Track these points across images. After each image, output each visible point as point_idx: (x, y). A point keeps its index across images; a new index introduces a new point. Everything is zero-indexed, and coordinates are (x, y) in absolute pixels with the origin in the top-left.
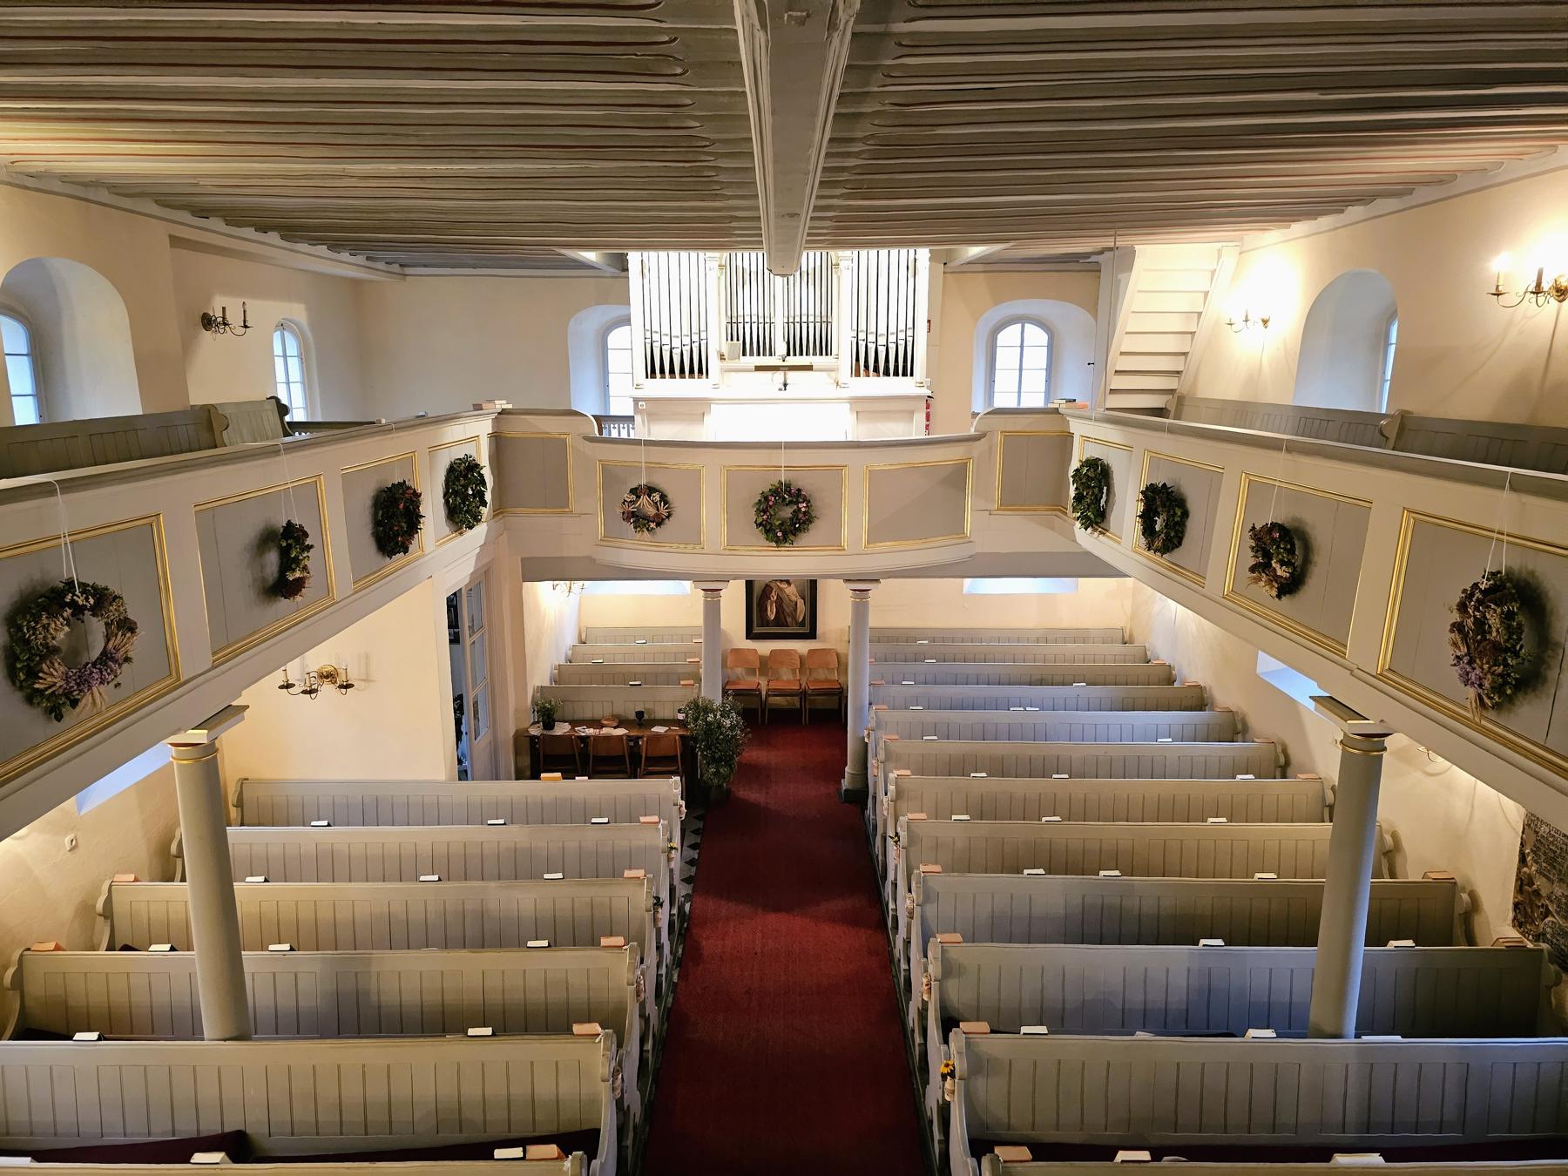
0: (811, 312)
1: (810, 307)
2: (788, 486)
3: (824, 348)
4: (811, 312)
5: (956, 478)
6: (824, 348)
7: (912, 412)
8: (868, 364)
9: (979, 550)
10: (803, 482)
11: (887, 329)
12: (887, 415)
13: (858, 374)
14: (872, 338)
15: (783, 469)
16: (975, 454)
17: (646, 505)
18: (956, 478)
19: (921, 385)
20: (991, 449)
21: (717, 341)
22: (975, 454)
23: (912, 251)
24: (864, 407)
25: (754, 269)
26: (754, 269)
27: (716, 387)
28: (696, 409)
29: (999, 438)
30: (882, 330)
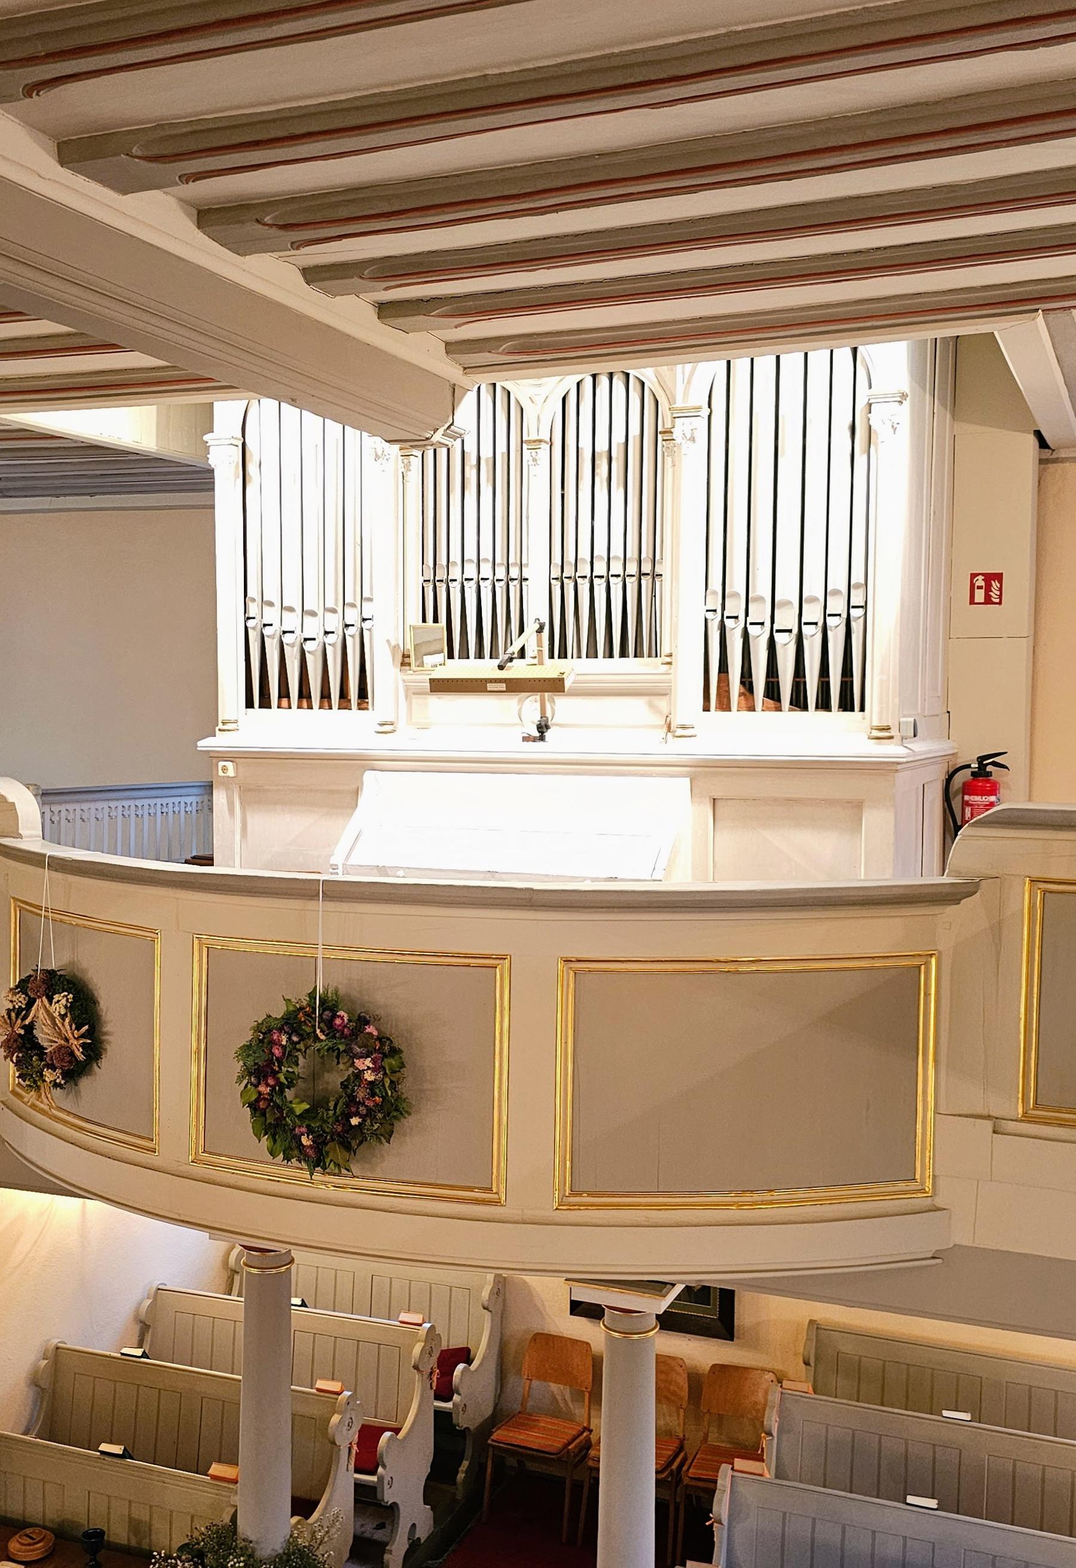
0: (617, 550)
1: (606, 530)
2: (329, 1005)
3: (633, 638)
4: (617, 550)
5: (882, 1012)
6: (633, 638)
7: (857, 806)
8: (744, 677)
9: (962, 1237)
10: (396, 1002)
11: (795, 587)
12: (790, 809)
13: (724, 705)
14: (760, 612)
15: (332, 953)
16: (945, 942)
17: (51, 1020)
18: (882, 1012)
19: (883, 734)
20: (997, 930)
21: (392, 616)
22: (945, 942)
23: (843, 355)
24: (729, 788)
25: (486, 453)
26: (486, 453)
27: (386, 727)
28: (331, 782)
29: (1023, 899)
30: (787, 591)
